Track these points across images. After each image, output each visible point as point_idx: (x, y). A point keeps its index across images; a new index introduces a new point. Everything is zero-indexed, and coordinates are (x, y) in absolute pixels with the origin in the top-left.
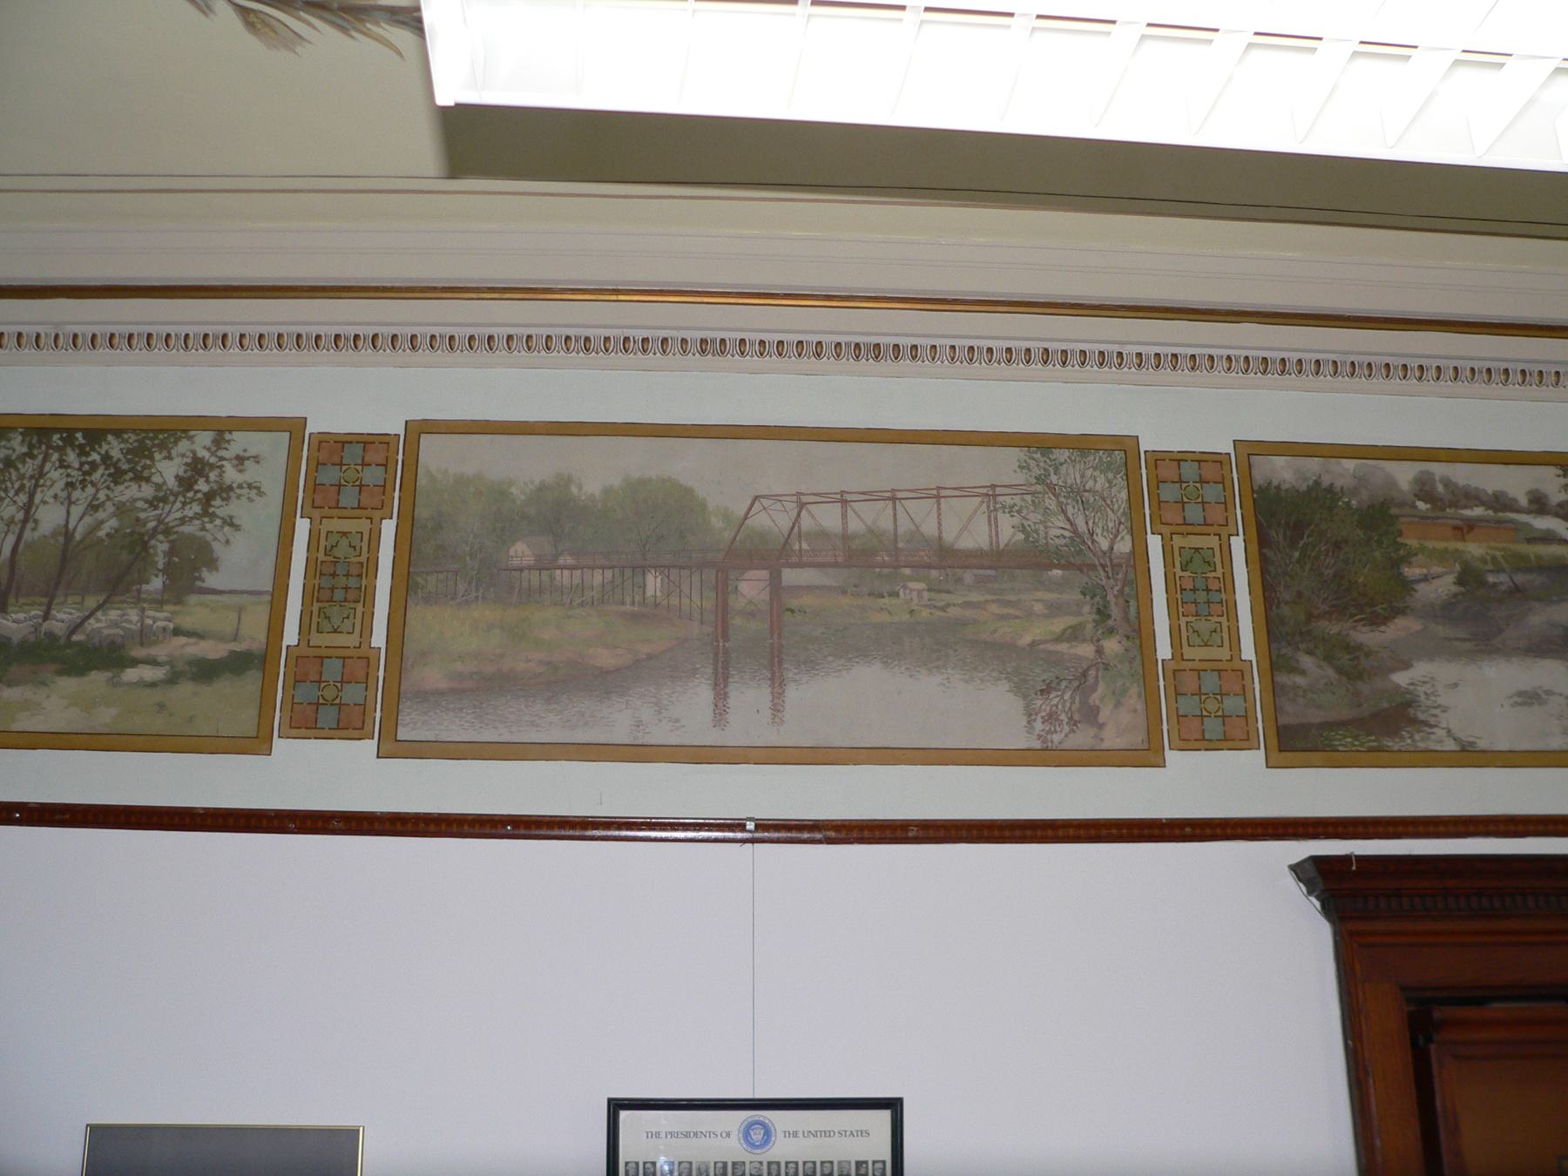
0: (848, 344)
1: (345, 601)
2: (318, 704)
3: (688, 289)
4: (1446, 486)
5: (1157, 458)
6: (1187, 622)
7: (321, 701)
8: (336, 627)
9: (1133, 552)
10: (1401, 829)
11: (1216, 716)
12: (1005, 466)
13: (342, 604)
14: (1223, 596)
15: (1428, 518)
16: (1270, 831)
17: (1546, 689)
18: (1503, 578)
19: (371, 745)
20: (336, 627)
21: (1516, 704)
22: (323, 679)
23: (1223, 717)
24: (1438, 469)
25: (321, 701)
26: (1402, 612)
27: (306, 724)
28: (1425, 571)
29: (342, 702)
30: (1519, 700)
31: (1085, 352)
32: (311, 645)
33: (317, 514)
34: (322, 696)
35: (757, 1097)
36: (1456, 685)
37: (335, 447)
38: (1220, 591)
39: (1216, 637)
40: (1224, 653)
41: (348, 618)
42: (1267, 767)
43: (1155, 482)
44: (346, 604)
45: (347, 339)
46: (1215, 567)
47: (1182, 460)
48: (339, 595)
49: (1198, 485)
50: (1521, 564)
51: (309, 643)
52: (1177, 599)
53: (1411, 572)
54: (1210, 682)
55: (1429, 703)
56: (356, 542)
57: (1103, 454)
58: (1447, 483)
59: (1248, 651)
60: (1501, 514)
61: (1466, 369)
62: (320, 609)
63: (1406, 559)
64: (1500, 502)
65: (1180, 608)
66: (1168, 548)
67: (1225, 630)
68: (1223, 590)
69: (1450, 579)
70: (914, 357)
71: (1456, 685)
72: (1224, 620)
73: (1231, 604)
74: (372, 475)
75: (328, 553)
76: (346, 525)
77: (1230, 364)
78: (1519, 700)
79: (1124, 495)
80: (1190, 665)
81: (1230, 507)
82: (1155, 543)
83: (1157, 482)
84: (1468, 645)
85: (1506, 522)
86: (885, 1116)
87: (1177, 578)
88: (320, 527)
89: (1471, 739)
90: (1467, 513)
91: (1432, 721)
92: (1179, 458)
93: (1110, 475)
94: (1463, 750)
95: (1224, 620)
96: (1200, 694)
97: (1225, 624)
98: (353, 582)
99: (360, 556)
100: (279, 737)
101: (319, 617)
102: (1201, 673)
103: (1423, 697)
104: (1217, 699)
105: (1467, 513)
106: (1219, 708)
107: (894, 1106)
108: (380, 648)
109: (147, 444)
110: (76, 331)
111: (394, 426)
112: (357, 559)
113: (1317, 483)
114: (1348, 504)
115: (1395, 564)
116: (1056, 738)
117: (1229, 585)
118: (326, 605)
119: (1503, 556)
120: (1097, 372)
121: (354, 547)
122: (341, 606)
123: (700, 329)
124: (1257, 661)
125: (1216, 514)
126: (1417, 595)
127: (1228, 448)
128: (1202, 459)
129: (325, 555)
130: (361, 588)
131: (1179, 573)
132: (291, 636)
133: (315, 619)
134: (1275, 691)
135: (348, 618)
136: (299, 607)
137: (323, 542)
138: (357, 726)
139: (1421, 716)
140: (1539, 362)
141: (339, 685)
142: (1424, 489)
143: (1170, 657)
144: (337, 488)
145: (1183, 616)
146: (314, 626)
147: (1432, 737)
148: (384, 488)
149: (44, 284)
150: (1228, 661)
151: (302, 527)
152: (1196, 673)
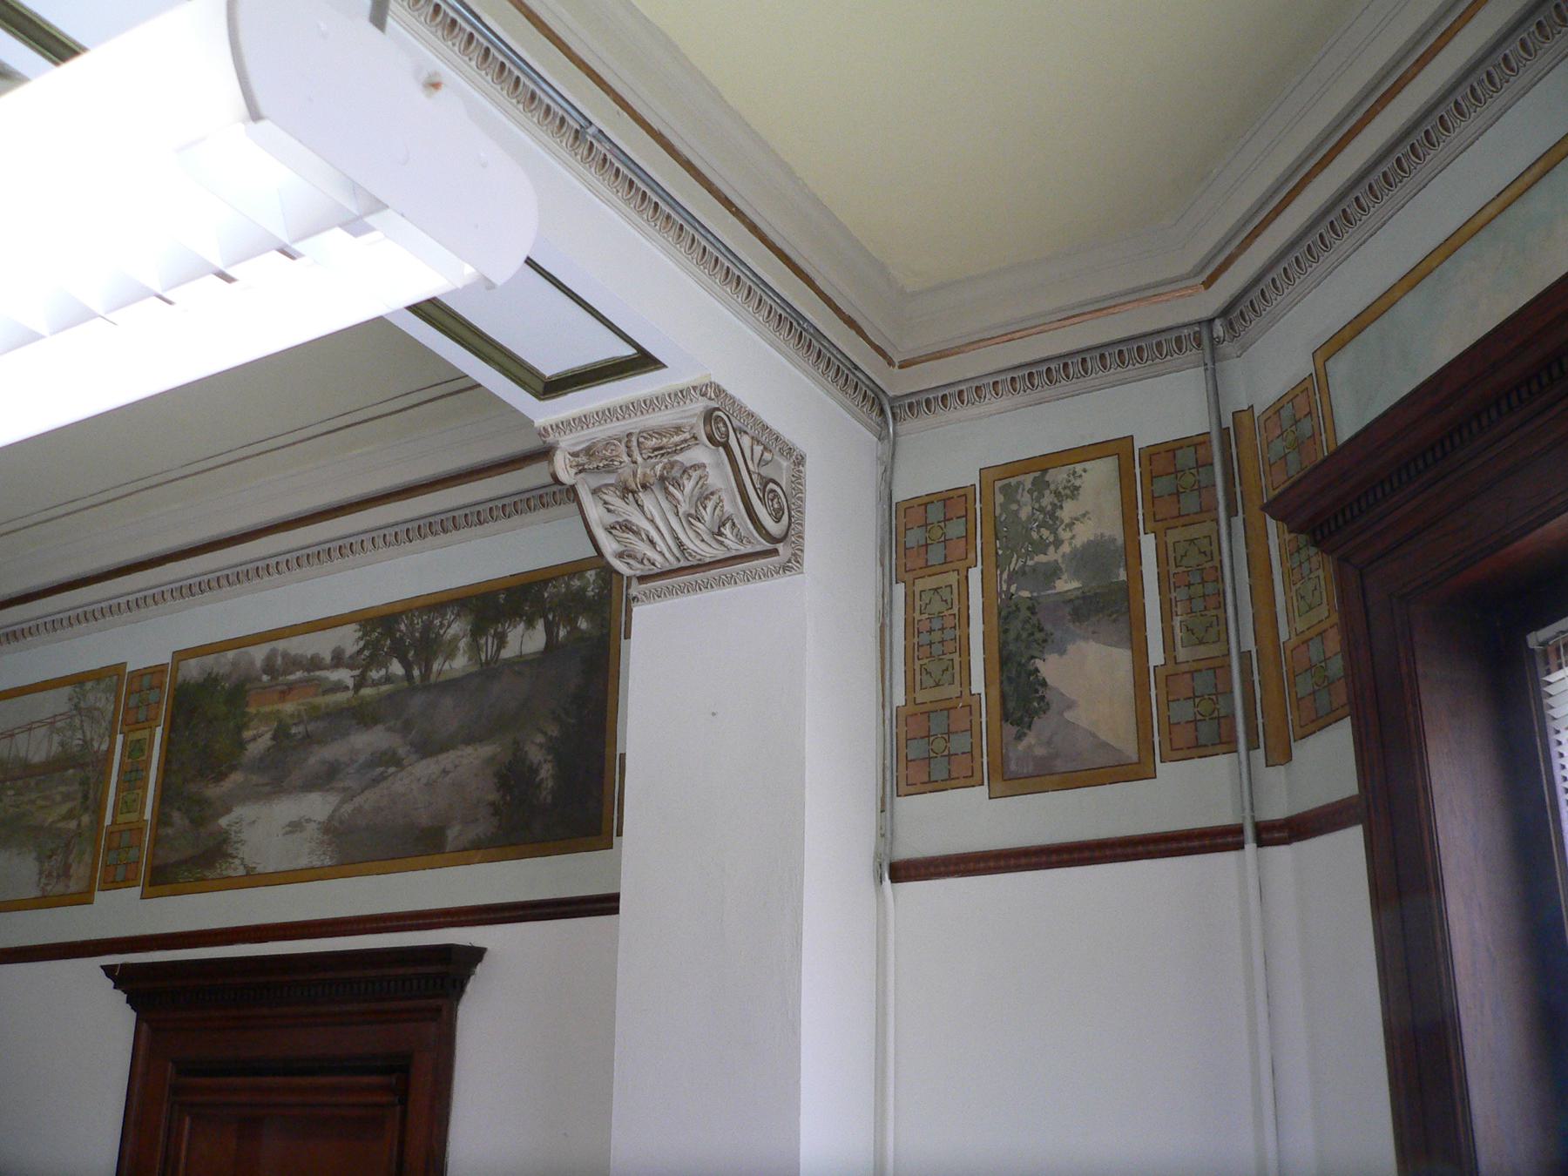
1: (943, 654)
2: (930, 758)
4: (283, 658)
7: (1199, 717)
8: (937, 680)
9: (108, 750)
10: (971, 866)
11: (1211, 719)
12: (56, 702)
13: (1203, 613)
15: (270, 687)
16: (942, 869)
17: (307, 818)
18: (301, 728)
20: (937, 680)
21: (287, 833)
22: (931, 734)
23: (949, 755)
24: (281, 645)
25: (1199, 717)
26: (233, 768)
28: (255, 732)
29: (951, 753)
30: (288, 829)
32: (917, 702)
36: (254, 822)
38: (955, 627)
39: (947, 676)
42: (1155, 777)
44: (1206, 612)
45: (58, 621)
50: (315, 714)
51: (915, 701)
52: (914, 644)
53: (247, 734)
55: (236, 839)
57: (794, 529)
58: (285, 655)
59: (148, 815)
60: (312, 674)
62: (921, 665)
63: (245, 726)
64: (315, 663)
66: (910, 593)
67: (957, 667)
68: (957, 628)
69: (268, 736)
71: (254, 822)
72: (956, 657)
74: (956, 529)
75: (923, 611)
78: (288, 829)
79: (112, 707)
80: (1185, 667)
82: (1148, 543)
84: (268, 788)
85: (313, 680)
87: (916, 622)
89: (254, 865)
90: (292, 677)
91: (234, 853)
93: (108, 695)
94: (248, 874)
98: (925, 638)
99: (952, 608)
100: (1161, 762)
103: (233, 833)
104: (1212, 700)
105: (292, 677)
106: (946, 747)
108: (980, 694)
109: (505, 599)
110: (192, 582)
111: (166, 658)
112: (950, 612)
113: (210, 674)
114: (223, 687)
115: (240, 729)
116: (49, 888)
118: (926, 661)
119: (305, 710)
121: (946, 601)
122: (1202, 615)
126: (247, 753)
129: (1177, 567)
130: (955, 638)
131: (1173, 570)
133: (918, 677)
134: (156, 840)
135: (1211, 626)
137: (918, 603)
139: (230, 851)
140: (373, 531)
141: (1214, 697)
142: (269, 668)
143: (1163, 663)
144: (924, 548)
147: (232, 866)
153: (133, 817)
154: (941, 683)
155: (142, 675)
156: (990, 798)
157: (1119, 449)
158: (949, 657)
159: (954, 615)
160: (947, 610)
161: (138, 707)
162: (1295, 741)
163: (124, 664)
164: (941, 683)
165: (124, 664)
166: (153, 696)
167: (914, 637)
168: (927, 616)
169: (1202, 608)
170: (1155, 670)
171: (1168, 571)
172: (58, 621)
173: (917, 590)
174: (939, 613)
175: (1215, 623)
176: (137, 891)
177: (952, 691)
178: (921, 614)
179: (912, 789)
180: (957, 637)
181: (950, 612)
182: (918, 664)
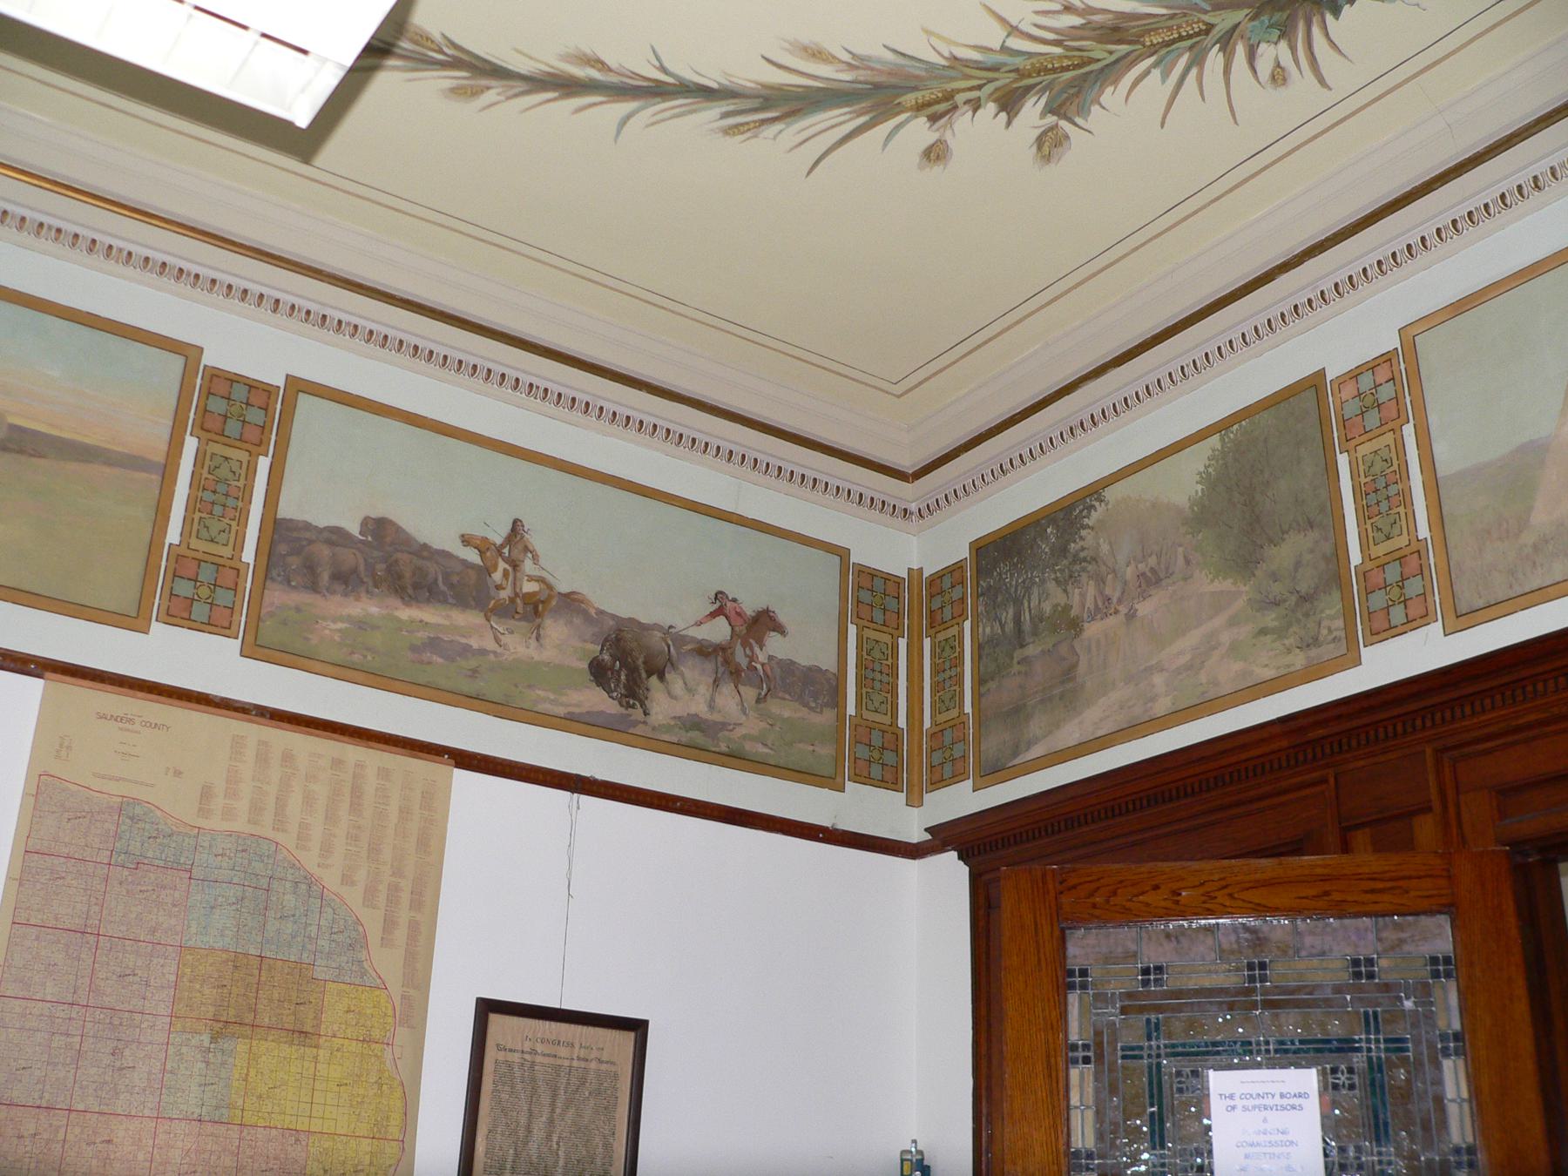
0: (348, 324)
2: (193, 599)
3: (34, 172)
5: (215, 375)
6: (201, 518)
7: (196, 597)
14: (240, 504)
16: (603, 790)
19: (208, 359)
25: (1390, 603)
27: (180, 615)
31: (418, 347)
33: (204, 435)
34: (197, 594)
35: (564, 1007)
37: (222, 382)
39: (213, 464)
40: (226, 552)
41: (224, 532)
43: (857, 588)
46: (239, 477)
47: (235, 381)
48: (218, 510)
49: (244, 406)
54: (206, 574)
56: (884, 650)
59: (248, 555)
61: (787, 471)
62: (201, 518)
65: (198, 503)
68: (240, 499)
70: (275, 311)
72: (234, 524)
73: (895, 686)
76: (229, 452)
77: (371, 337)
81: (901, 617)
83: (208, 393)
86: (629, 1038)
87: (1362, 485)
88: (250, 458)
92: (233, 379)
95: (234, 524)
96: (196, 581)
97: (234, 527)
101: (199, 525)
102: (202, 563)
107: (638, 1028)
111: (1392, 342)
112: (1392, 469)
117: (247, 496)
120: (524, 398)
121: (1386, 460)
123: (147, 247)
124: (255, 566)
125: (252, 434)
127: (279, 381)
128: (253, 386)
131: (205, 475)
132: (173, 535)
136: (248, 531)
137: (207, 462)
138: (224, 625)
145: (199, 511)
146: (194, 534)
148: (264, 429)
149: (860, 455)
150: (228, 558)
151: (852, 630)
152: (197, 562)
153: (954, 713)
154: (1391, 536)
155: (941, 577)
156: (1445, 635)
157: (188, 353)
158: (1395, 510)
159: (1395, 471)
160: (1388, 468)
161: (942, 608)
162: (926, 793)
163: (1321, 373)
164: (1391, 536)
165: (1321, 373)
166: (956, 593)
167: (198, 490)
168: (1372, 478)
169: (1388, 509)
170: (169, 547)
171: (201, 474)
172: (1511, 194)
173: (1360, 455)
174: (1382, 472)
175: (1398, 519)
176: (969, 783)
177: (1402, 541)
178: (1366, 477)
179: (1376, 638)
180: (239, 509)
181: (1392, 469)
182: (197, 515)
